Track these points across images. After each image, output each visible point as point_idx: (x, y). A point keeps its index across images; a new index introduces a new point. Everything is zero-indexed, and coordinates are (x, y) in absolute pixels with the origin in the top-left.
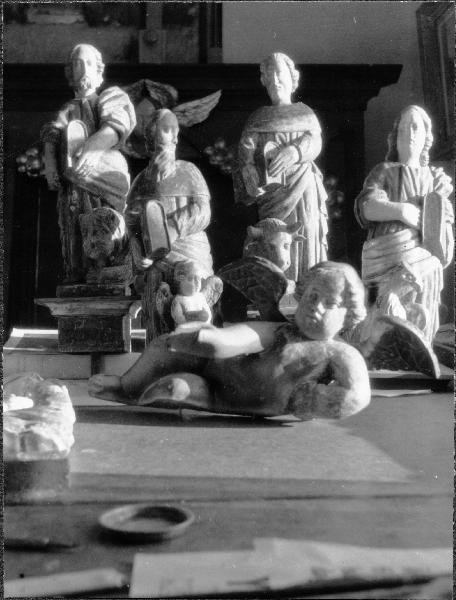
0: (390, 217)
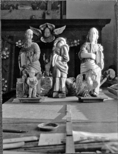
0: (88, 57)
